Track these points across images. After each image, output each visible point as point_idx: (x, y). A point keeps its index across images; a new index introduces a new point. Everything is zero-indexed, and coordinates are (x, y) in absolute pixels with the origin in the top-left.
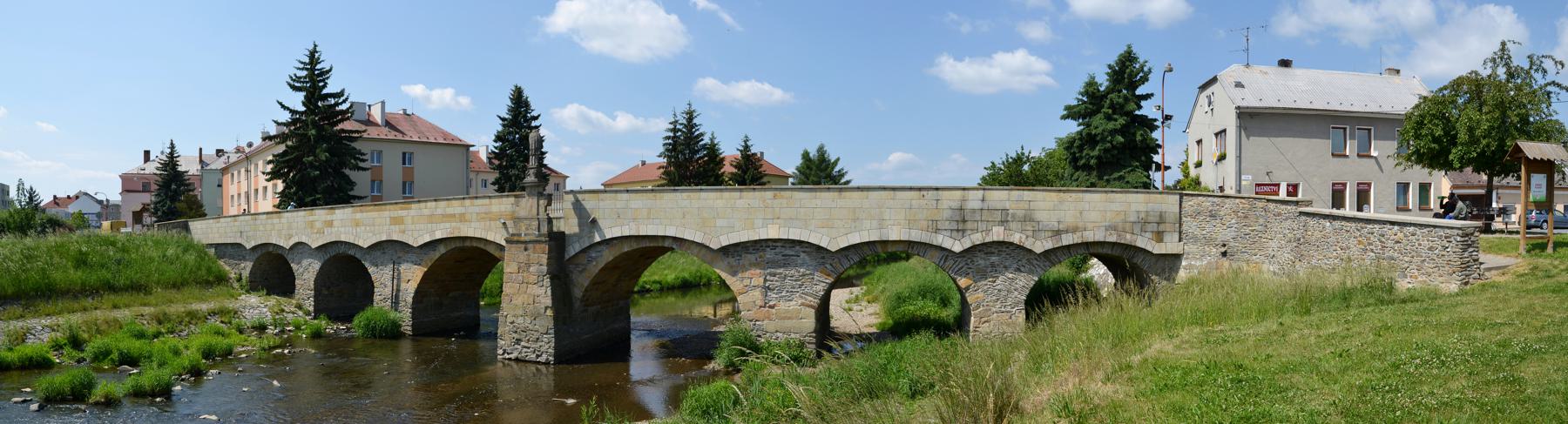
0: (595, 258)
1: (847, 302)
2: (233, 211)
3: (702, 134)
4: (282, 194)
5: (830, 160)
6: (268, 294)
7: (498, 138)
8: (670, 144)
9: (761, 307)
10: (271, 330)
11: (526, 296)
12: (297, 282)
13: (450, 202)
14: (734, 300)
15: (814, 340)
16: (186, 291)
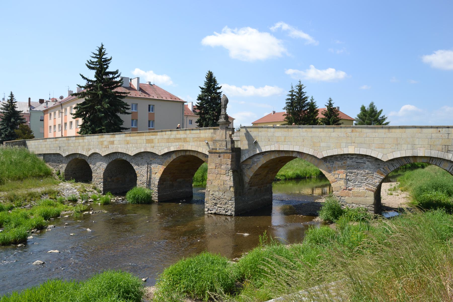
0: (256, 162)
1: (389, 190)
2: (51, 135)
3: (306, 98)
4: (83, 126)
5: (376, 111)
6: (77, 181)
7: (199, 98)
8: (289, 103)
9: (344, 190)
10: (80, 201)
11: (220, 181)
12: (93, 174)
13: (178, 132)
14: (330, 185)
15: (373, 209)
16: (27, 182)
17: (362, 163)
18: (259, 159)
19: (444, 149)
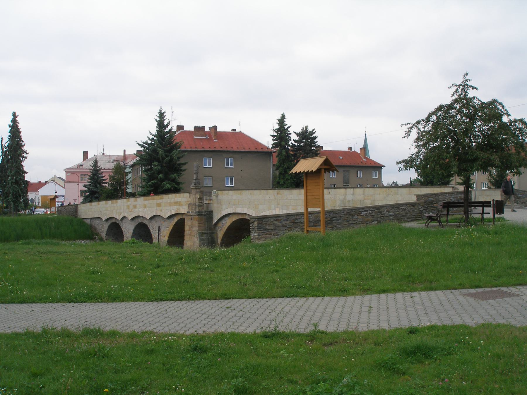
18: (226, 222)
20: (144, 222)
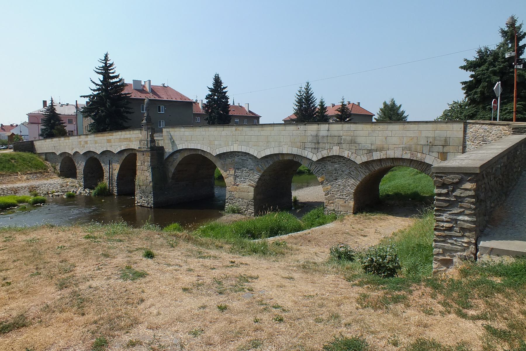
12: (77, 171)
17: (245, 160)
18: (177, 157)
19: (302, 146)
20: (95, 156)
